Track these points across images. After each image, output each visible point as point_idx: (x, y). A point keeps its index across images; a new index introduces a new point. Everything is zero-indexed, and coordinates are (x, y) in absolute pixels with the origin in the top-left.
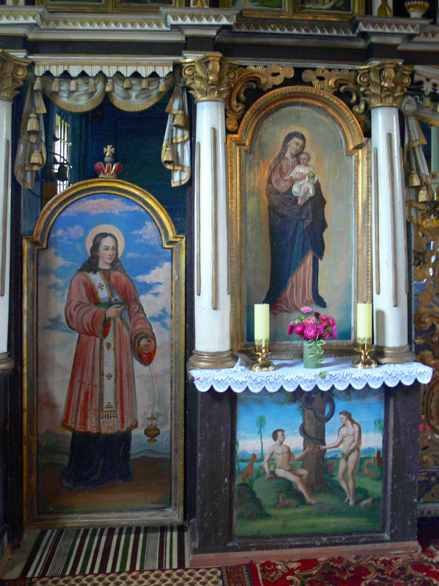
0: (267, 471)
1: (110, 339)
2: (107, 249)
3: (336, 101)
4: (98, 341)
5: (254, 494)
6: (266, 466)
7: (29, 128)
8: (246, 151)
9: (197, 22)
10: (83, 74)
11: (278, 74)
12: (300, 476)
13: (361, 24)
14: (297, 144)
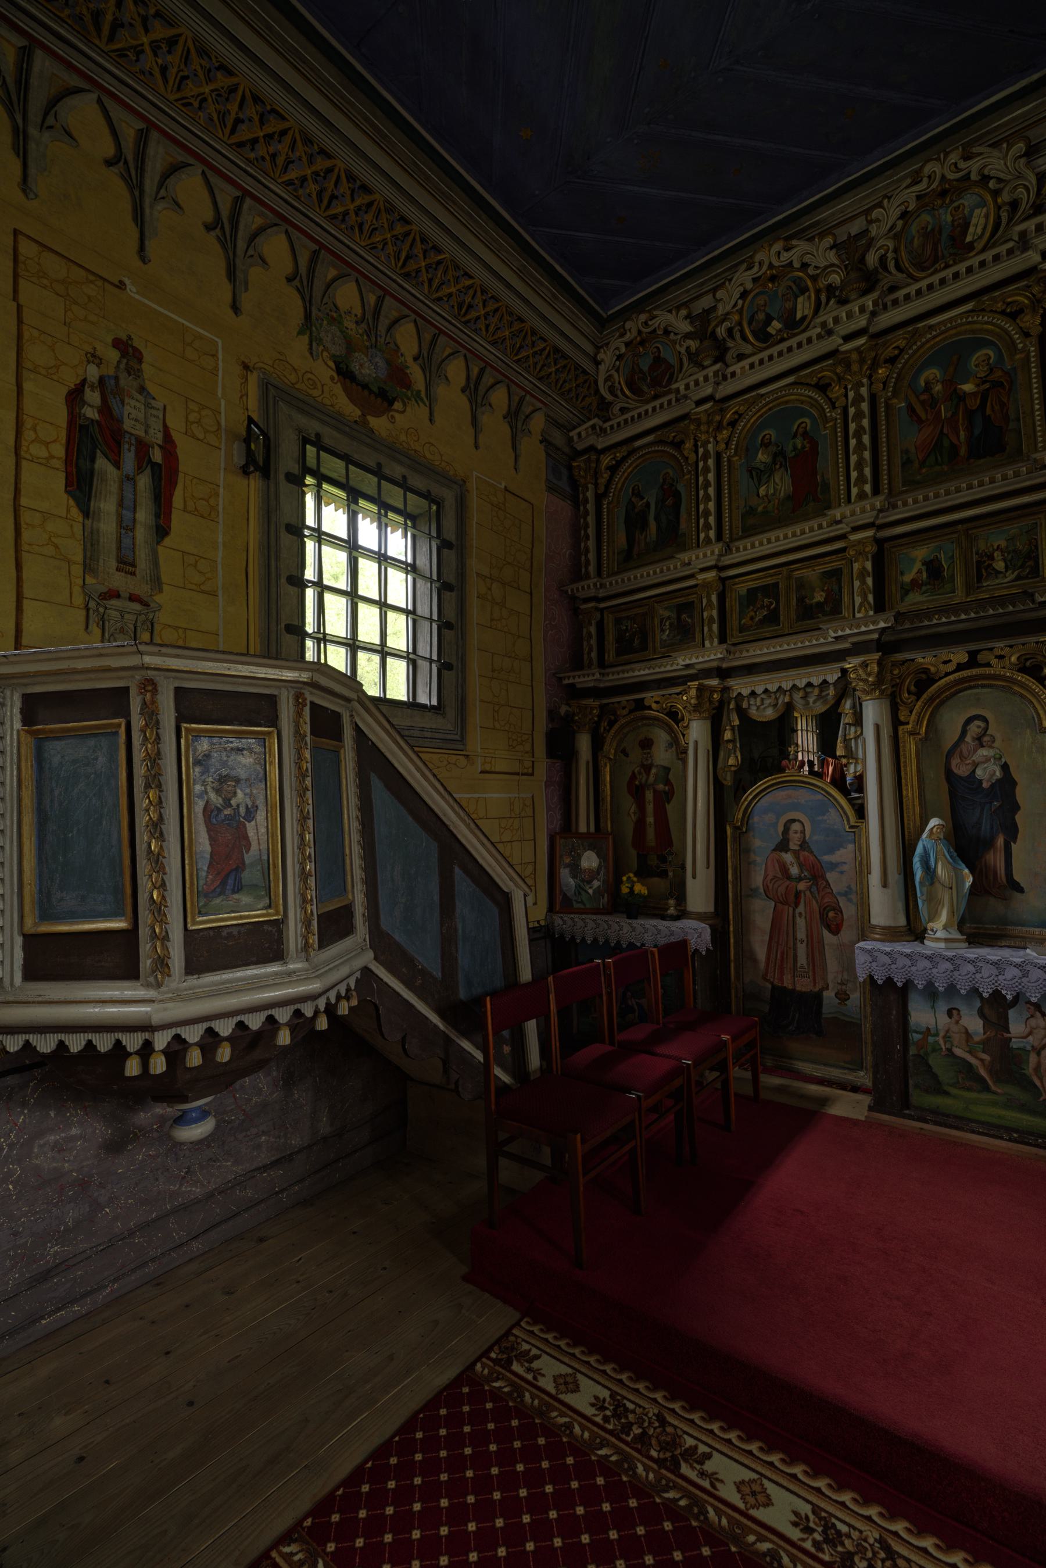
0: (944, 1047)
1: (801, 908)
2: (796, 832)
3: (1020, 677)
4: (791, 910)
5: (930, 1067)
6: (941, 1042)
7: (726, 738)
8: (921, 740)
9: (856, 631)
10: (766, 691)
11: (950, 661)
12: (982, 1060)
13: (1037, 594)
14: (979, 727)
